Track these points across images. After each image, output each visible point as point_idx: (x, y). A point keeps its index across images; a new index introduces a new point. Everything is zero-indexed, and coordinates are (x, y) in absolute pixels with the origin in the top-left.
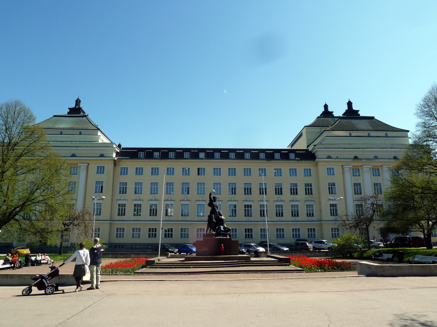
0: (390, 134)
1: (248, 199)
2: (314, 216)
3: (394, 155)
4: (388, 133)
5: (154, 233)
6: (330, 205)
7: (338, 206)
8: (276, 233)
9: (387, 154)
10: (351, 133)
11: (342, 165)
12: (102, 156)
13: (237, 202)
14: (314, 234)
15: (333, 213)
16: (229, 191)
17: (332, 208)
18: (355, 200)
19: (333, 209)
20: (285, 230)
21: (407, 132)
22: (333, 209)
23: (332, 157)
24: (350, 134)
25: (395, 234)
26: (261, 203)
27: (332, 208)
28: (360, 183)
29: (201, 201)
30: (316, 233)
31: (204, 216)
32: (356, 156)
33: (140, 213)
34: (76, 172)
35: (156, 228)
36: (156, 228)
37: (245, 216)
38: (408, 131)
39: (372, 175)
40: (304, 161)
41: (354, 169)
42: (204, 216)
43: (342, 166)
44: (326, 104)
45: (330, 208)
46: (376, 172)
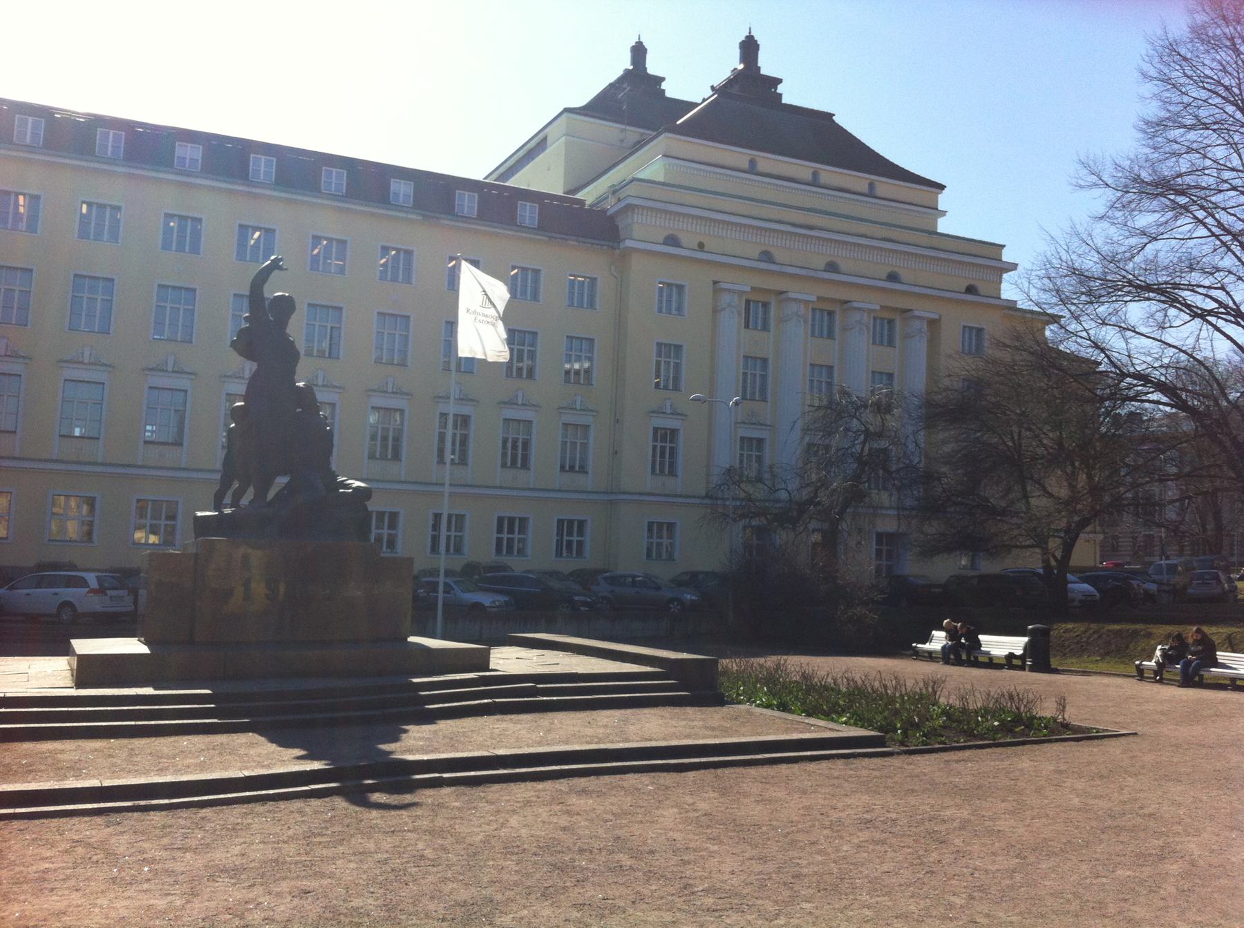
0: (886, 186)
1: (87, 354)
2: (587, 473)
3: (892, 265)
4: (876, 183)
5: (575, 538)
6: (656, 430)
7: (681, 438)
8: (495, 535)
9: (814, 252)
10: (758, 159)
11: (716, 279)
12: (971, 290)
13: (193, 377)
14: (580, 544)
15: (662, 464)
16: (155, 322)
17: (659, 444)
18: (739, 421)
19: (663, 449)
20: (401, 519)
21: (936, 190)
22: (663, 449)
23: (684, 245)
24: (815, 174)
25: (961, 554)
26: (442, 408)
27: (659, 444)
28: (891, 372)
29: (520, 407)
30: (587, 539)
31: (98, 439)
32: (672, 235)
33: (452, 457)
34: (527, 279)
35: (398, 513)
36: (398, 513)
37: (504, 465)
38: (942, 187)
39: (871, 342)
40: (576, 241)
41: (334, 242)
42: (98, 439)
43: (715, 283)
44: (753, 36)
45: (651, 443)
46: (583, 290)
